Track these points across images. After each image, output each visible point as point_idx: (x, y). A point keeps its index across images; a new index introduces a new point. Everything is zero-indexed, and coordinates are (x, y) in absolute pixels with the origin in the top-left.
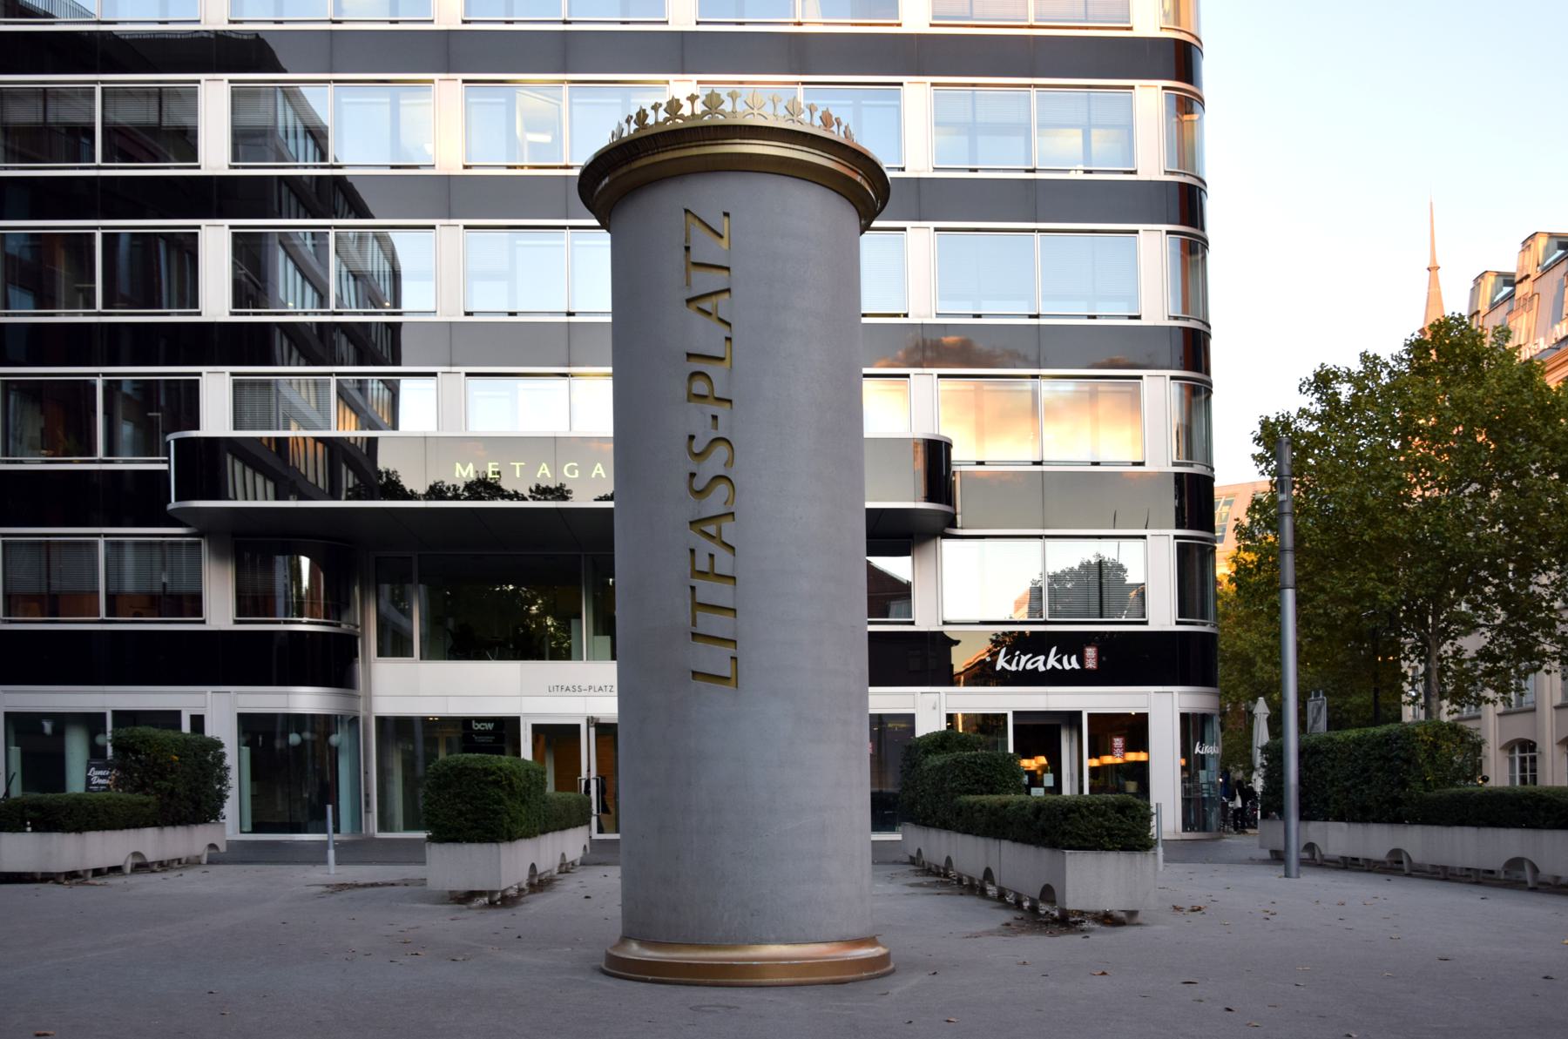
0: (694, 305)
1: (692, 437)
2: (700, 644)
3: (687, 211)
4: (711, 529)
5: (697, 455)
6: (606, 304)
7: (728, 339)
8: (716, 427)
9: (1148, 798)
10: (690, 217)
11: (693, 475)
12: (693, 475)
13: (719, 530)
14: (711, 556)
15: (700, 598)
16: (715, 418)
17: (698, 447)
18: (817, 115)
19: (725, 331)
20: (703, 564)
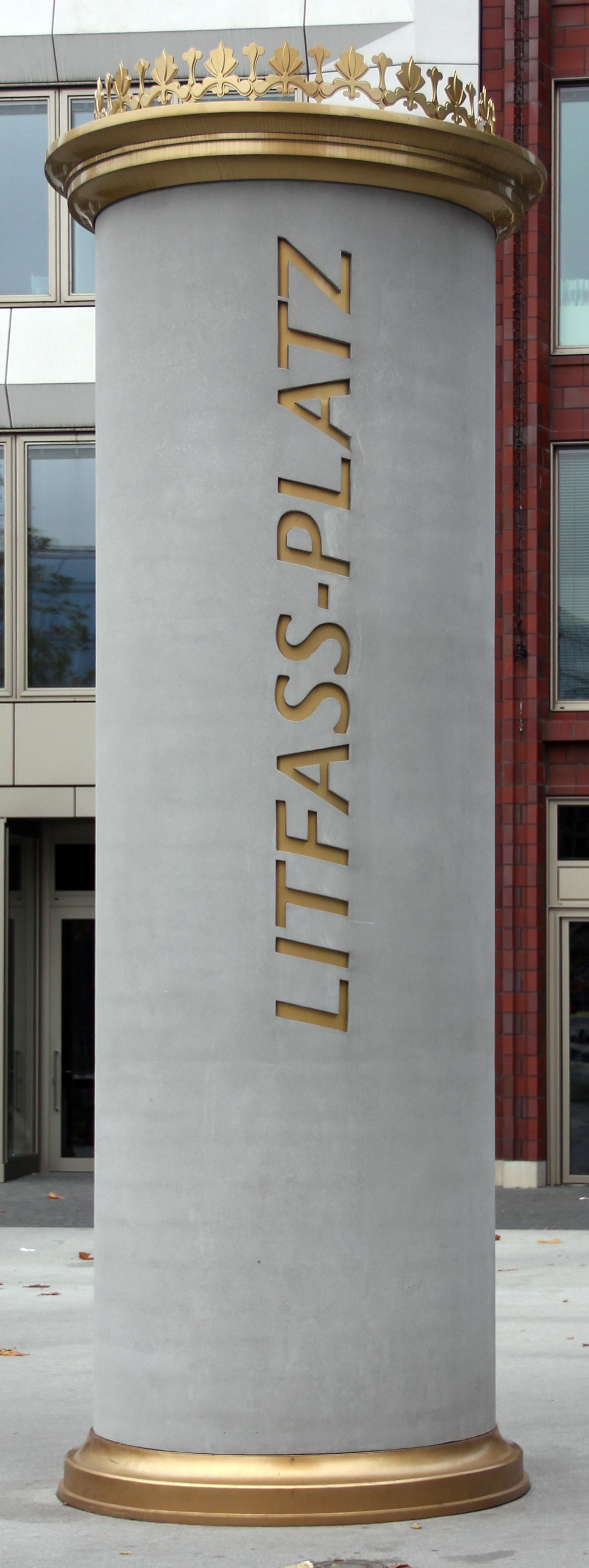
0: (289, 401)
1: (284, 618)
2: (345, 559)
3: (281, 240)
4: (312, 770)
5: (293, 708)
6: (507, 1298)
7: (346, 461)
8: (324, 602)
9: (538, 428)
10: (285, 250)
11: (282, 679)
12: (282, 679)
13: (326, 775)
14: (312, 814)
15: (292, 882)
16: (323, 587)
17: (295, 633)
18: (443, 84)
19: (342, 451)
20: (298, 827)
